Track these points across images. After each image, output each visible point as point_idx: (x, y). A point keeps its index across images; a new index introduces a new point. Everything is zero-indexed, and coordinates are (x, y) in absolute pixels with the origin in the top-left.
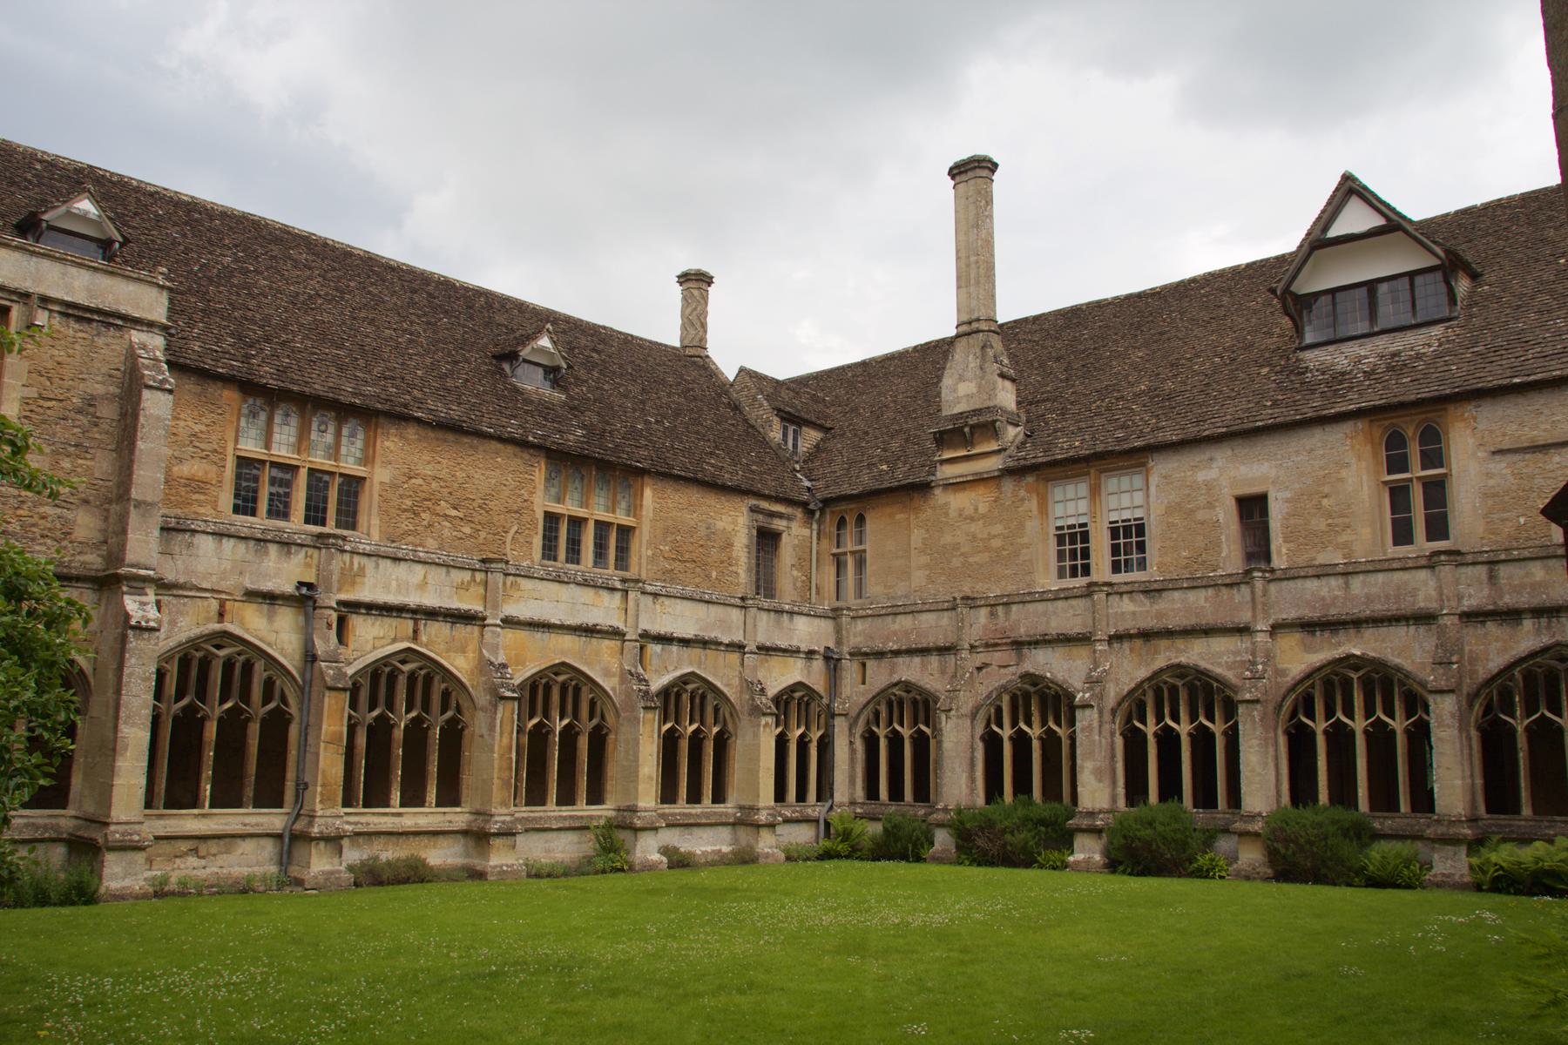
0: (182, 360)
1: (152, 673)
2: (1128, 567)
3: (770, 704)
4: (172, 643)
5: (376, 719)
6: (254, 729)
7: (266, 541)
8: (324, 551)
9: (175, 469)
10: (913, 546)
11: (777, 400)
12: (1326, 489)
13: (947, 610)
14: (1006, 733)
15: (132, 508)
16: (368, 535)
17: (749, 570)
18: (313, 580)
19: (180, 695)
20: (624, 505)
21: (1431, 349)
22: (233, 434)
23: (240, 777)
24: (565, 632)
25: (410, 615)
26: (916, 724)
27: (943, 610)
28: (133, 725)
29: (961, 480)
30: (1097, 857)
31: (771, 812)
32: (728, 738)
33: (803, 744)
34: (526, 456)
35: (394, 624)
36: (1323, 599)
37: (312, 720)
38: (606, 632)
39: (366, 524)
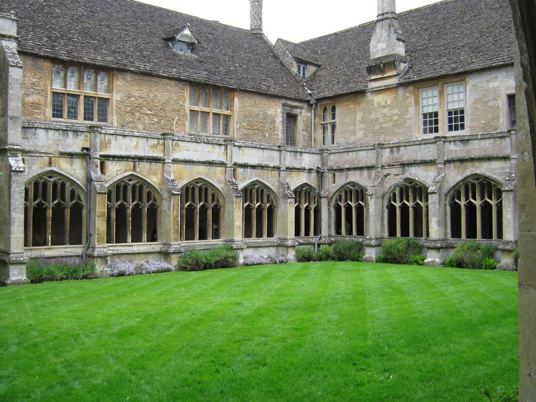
0: (25, 50)
1: (23, 190)
2: (456, 129)
3: (292, 193)
4: (30, 176)
5: (119, 205)
6: (68, 212)
7: (67, 131)
8: (92, 134)
9: (26, 99)
10: (357, 120)
11: (295, 53)
13: (371, 150)
14: (397, 205)
15: (9, 119)
16: (112, 124)
17: (283, 133)
18: (88, 147)
19: (35, 199)
20: (225, 105)
22: (50, 82)
23: (63, 231)
24: (200, 164)
25: (131, 160)
26: (357, 201)
27: (369, 150)
29: (379, 89)
30: (438, 260)
31: (293, 240)
32: (274, 209)
33: (307, 210)
34: (181, 85)
35: (125, 164)
37: (92, 207)
38: (218, 164)
39: (111, 120)
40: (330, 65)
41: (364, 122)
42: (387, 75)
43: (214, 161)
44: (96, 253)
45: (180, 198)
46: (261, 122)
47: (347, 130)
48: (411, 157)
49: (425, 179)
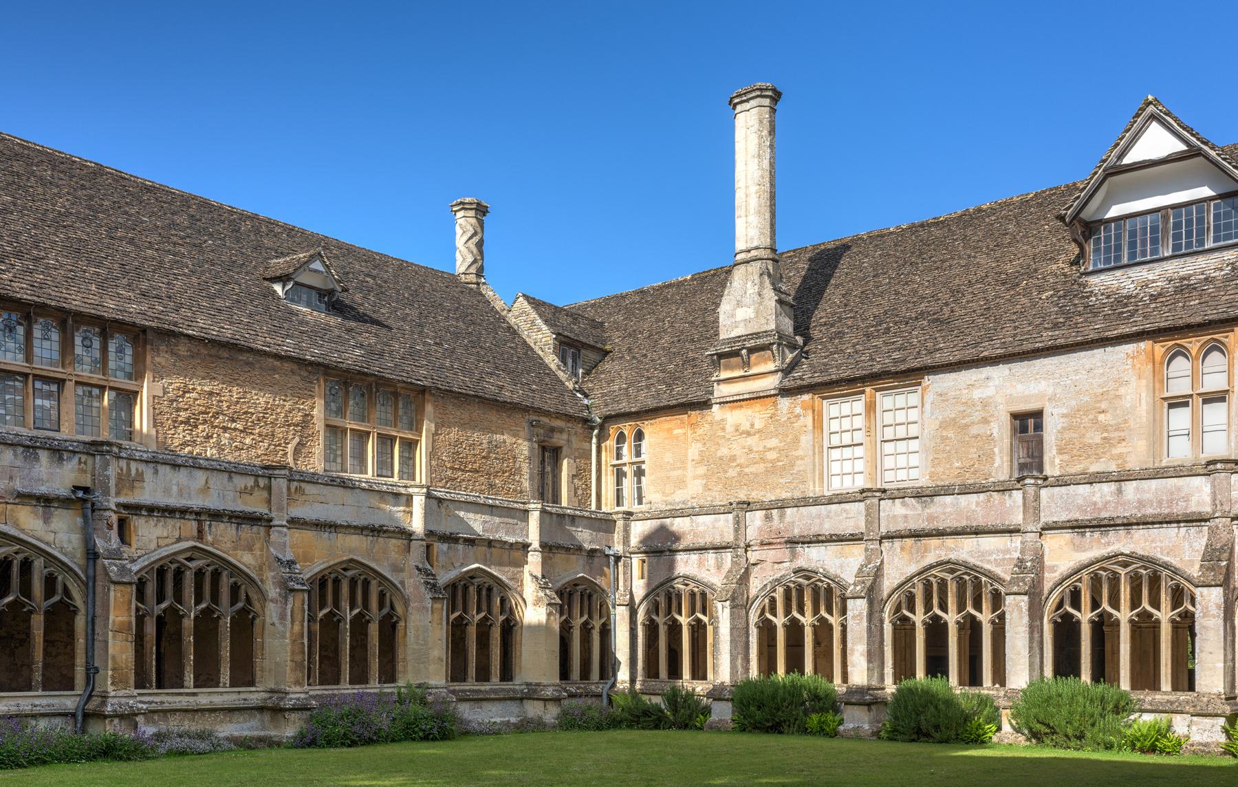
7: (35, 448)
8: (98, 458)
10: (690, 458)
12: (1104, 406)
14: (780, 621)
17: (531, 479)
18: (89, 484)
21: (1223, 273)
31: (557, 688)
35: (178, 525)
36: (1095, 504)
37: (99, 611)
40: (630, 349)
42: (752, 372)
43: (384, 526)
44: (109, 709)
45: (306, 599)
48: (810, 529)
49: (838, 572)
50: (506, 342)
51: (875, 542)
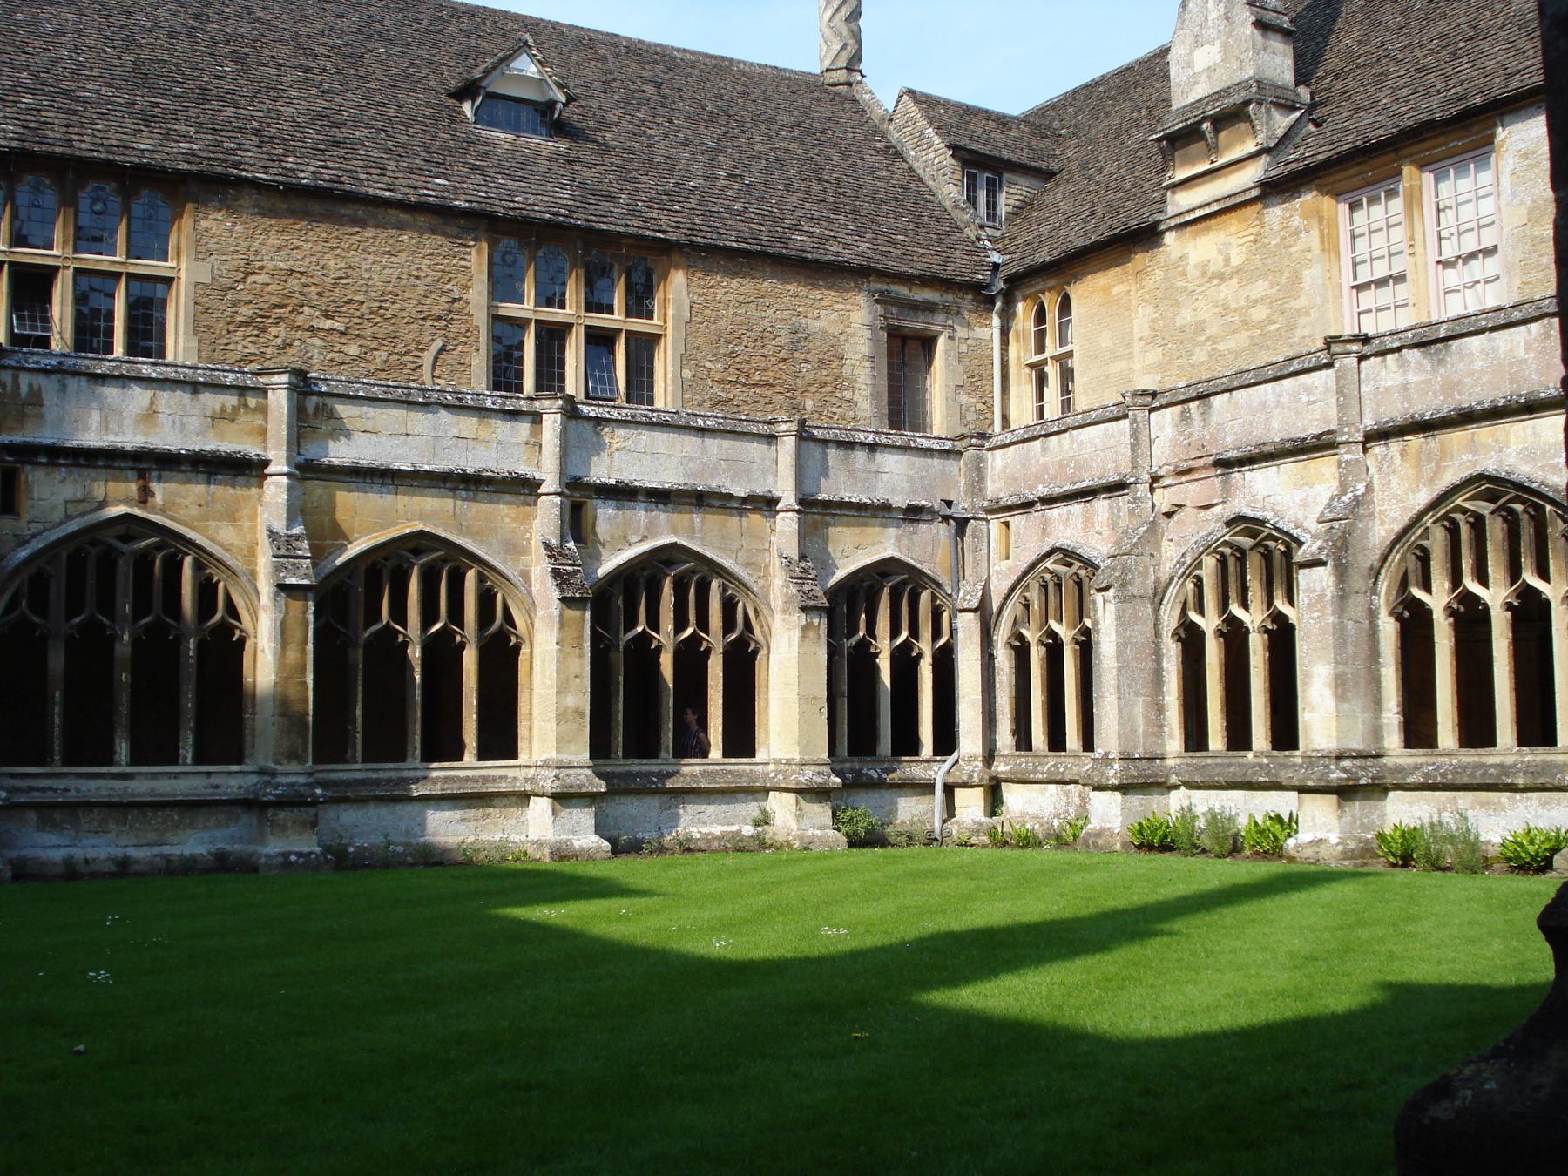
10: (1137, 336)
17: (875, 395)
25: (130, 464)
28: (1167, 805)
41: (1160, 341)
42: (1221, 161)
46: (784, 360)
47: (1107, 376)
50: (873, 169)
51: (1353, 447)
